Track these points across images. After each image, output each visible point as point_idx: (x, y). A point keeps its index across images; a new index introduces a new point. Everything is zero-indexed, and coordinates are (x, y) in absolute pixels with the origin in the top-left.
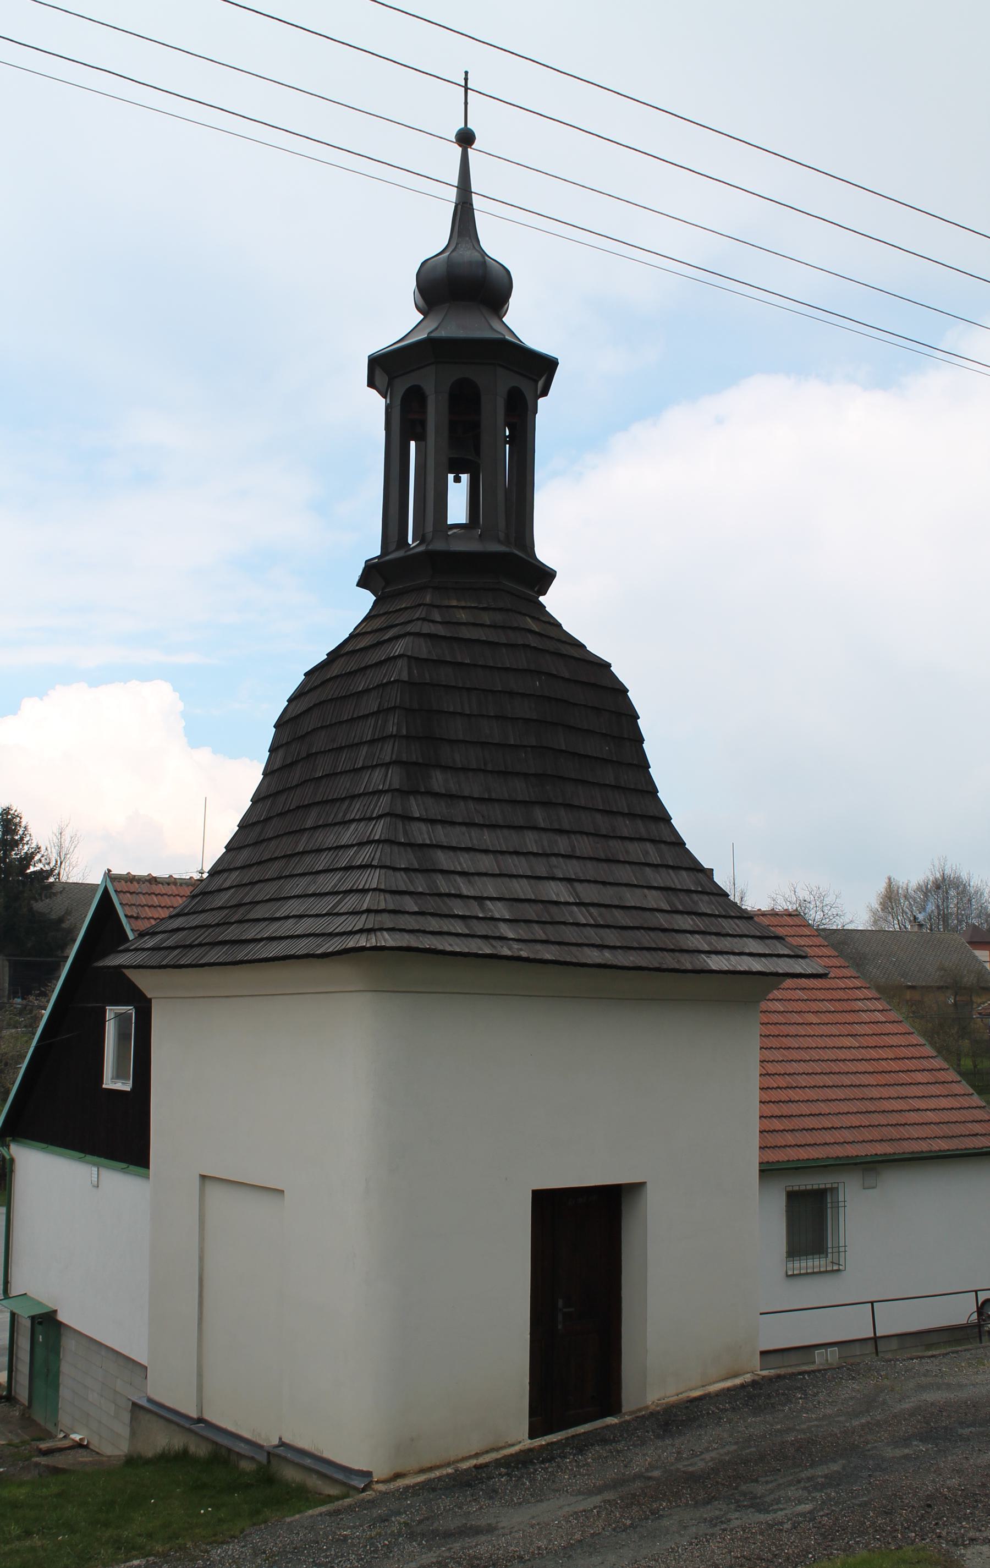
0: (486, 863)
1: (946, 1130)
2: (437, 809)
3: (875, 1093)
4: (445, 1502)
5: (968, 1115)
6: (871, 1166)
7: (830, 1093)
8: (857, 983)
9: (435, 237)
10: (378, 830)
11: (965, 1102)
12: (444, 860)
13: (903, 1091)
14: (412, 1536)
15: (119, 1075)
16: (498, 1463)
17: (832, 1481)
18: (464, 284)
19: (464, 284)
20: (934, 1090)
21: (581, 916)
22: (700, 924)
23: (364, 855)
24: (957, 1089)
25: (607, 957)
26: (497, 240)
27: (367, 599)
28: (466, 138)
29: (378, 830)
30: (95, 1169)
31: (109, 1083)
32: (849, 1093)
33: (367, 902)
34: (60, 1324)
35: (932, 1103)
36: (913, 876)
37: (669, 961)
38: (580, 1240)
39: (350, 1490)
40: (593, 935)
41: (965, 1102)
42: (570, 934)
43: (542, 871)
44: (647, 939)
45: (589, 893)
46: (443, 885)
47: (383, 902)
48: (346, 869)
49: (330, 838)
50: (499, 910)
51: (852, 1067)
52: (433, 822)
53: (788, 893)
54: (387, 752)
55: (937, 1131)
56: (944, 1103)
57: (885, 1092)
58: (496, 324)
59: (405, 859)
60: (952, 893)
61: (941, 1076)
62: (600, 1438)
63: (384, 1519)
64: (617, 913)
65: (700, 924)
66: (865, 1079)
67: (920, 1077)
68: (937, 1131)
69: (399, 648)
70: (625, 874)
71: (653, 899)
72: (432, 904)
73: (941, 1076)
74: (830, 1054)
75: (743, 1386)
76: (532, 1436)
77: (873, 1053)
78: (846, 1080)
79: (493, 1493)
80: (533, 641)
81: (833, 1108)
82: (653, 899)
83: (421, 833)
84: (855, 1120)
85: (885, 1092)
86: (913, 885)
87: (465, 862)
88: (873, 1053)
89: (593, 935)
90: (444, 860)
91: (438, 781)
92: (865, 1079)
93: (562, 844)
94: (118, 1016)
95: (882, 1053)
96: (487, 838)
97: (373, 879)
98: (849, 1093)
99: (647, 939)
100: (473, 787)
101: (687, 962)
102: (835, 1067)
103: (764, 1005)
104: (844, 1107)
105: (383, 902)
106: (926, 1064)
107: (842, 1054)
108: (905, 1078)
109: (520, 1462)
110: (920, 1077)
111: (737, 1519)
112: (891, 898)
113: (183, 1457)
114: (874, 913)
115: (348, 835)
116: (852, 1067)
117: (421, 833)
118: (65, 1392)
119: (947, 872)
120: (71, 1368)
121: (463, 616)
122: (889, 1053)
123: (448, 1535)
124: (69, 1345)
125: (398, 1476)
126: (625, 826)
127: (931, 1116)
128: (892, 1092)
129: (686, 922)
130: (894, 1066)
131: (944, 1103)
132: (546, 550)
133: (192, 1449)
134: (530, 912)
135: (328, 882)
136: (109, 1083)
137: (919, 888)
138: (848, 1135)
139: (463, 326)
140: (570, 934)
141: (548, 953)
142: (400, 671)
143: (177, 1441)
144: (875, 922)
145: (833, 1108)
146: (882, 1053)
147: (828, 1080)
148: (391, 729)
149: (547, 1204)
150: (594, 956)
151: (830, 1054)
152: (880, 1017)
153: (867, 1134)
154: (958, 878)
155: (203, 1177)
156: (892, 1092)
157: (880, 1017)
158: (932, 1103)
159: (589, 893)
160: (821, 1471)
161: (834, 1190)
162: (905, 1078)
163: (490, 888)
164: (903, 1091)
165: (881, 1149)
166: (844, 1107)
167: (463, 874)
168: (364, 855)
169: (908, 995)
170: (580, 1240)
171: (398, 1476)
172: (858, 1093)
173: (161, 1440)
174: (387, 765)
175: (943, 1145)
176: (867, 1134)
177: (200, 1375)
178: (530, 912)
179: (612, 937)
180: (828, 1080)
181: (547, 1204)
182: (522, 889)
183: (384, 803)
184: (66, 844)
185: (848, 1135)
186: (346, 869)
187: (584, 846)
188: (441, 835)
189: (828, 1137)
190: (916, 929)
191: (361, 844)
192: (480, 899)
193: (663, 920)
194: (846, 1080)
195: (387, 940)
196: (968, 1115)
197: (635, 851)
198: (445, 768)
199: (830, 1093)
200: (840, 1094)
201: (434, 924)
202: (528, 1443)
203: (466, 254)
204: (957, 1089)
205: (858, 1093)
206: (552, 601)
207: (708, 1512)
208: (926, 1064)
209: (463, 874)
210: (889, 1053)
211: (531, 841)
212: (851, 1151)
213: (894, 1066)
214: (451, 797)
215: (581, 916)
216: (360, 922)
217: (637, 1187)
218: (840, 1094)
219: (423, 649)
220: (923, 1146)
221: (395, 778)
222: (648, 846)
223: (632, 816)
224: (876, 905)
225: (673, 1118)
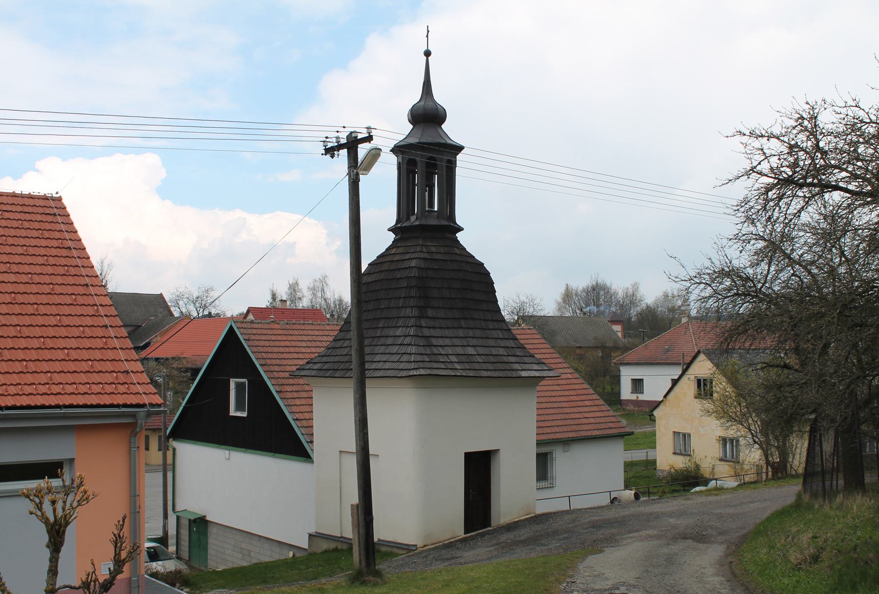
0: (447, 342)
1: (599, 426)
2: (431, 323)
3: (568, 410)
4: (443, 552)
5: (608, 419)
6: (567, 442)
7: (550, 411)
8: (560, 361)
9: (414, 96)
10: (412, 331)
11: (606, 414)
12: (434, 342)
13: (580, 409)
14: (437, 560)
15: (239, 407)
16: (456, 541)
17: (564, 539)
18: (428, 116)
19: (428, 116)
20: (594, 409)
21: (479, 359)
22: (517, 359)
23: (407, 340)
24: (603, 408)
25: (489, 374)
26: (440, 96)
27: (392, 237)
28: (428, 54)
29: (412, 331)
30: (227, 452)
31: (233, 412)
32: (557, 411)
33: (413, 358)
34: (208, 521)
35: (592, 415)
36: (581, 283)
37: (509, 374)
38: (479, 467)
39: (410, 551)
40: (484, 366)
41: (606, 414)
42: (477, 366)
43: (466, 344)
44: (501, 366)
45: (481, 351)
46: (435, 351)
47: (419, 358)
48: (401, 345)
49: (391, 332)
50: (454, 359)
51: (558, 399)
52: (429, 328)
53: (515, 298)
54: (412, 302)
55: (595, 427)
56: (598, 414)
57: (573, 410)
58: (439, 130)
59: (422, 342)
60: (602, 293)
61: (597, 402)
62: (488, 533)
63: (426, 557)
64: (491, 357)
65: (517, 359)
66: (564, 405)
67: (587, 403)
68: (595, 427)
69: (413, 263)
70: (491, 342)
71: (502, 351)
72: (433, 358)
73: (597, 402)
74: (548, 394)
75: (531, 517)
76: (466, 532)
77: (567, 393)
78: (556, 405)
79: (458, 549)
80: (459, 258)
81: (551, 417)
82: (502, 351)
83: (426, 332)
84: (560, 423)
85: (573, 410)
86: (580, 288)
87: (441, 342)
88: (567, 393)
89: (484, 366)
90: (434, 342)
91: (430, 313)
92: (564, 405)
93: (471, 333)
94: (236, 383)
95: (571, 393)
96: (447, 332)
97: (413, 349)
98: (557, 411)
99: (501, 366)
100: (441, 314)
101: (514, 374)
102: (551, 399)
103: (538, 388)
104: (555, 417)
105: (419, 358)
106: (590, 397)
107: (553, 394)
108: (581, 403)
109: (464, 540)
110: (587, 403)
111: (538, 549)
112: (568, 296)
113: (336, 550)
114: (559, 304)
115: (399, 332)
116: (558, 399)
117: (426, 332)
118: (211, 551)
119: (599, 281)
120: (214, 540)
121: (434, 249)
122: (574, 393)
123: (448, 559)
124: (212, 531)
125: (425, 546)
126: (491, 325)
127: (592, 420)
128: (575, 410)
129: (512, 359)
130: (576, 398)
131: (598, 414)
132: (459, 220)
133: (339, 547)
134: (463, 359)
135: (395, 349)
136: (233, 412)
137: (584, 290)
138: (557, 429)
139: (429, 137)
140: (477, 366)
141: (471, 373)
142: (414, 273)
143: (332, 545)
144: (559, 309)
145: (551, 417)
146: (571, 393)
147: (548, 405)
148: (413, 294)
149: (469, 456)
150: (484, 374)
151: (548, 394)
152: (570, 376)
153: (565, 429)
154: (605, 285)
155: (341, 452)
156: (575, 410)
157: (570, 376)
158: (592, 415)
159: (481, 351)
160: (561, 537)
161: (551, 453)
162: (581, 403)
163: (450, 351)
164: (580, 409)
165: (573, 435)
166: (555, 417)
167: (441, 346)
168: (407, 340)
169: (578, 351)
170: (479, 467)
171: (425, 546)
172: (561, 411)
173: (325, 545)
174: (412, 307)
175: (597, 433)
176: (565, 429)
177: (341, 521)
178: (463, 359)
179: (490, 366)
180: (548, 405)
181: (469, 456)
182: (460, 350)
183: (412, 322)
184: (105, 269)
185: (557, 429)
186: (401, 345)
187: (478, 333)
188: (433, 332)
189: (549, 430)
190: (582, 315)
191: (405, 336)
192: (447, 355)
193: (505, 359)
194: (556, 405)
195: (422, 372)
196: (608, 419)
197: (494, 334)
198: (432, 308)
199: (550, 411)
200: (553, 411)
201: (435, 365)
202: (464, 536)
203: (430, 104)
204: (603, 408)
205: (561, 411)
206: (459, 236)
207: (530, 547)
208: (590, 397)
209: (441, 346)
210: (574, 393)
211: (461, 333)
212: (558, 436)
213: (576, 398)
214: (434, 318)
215: (479, 359)
216: (413, 366)
217: (497, 451)
218: (553, 411)
219: (422, 264)
220: (589, 433)
221: (415, 312)
222: (499, 332)
223: (492, 320)
224: (560, 300)
225: (506, 425)
